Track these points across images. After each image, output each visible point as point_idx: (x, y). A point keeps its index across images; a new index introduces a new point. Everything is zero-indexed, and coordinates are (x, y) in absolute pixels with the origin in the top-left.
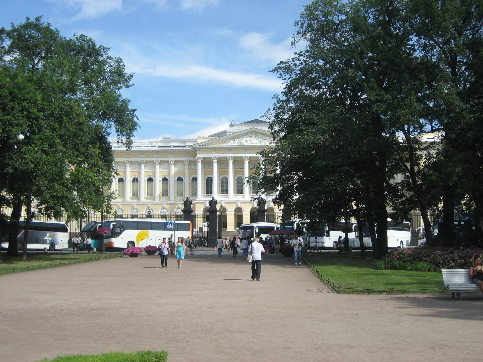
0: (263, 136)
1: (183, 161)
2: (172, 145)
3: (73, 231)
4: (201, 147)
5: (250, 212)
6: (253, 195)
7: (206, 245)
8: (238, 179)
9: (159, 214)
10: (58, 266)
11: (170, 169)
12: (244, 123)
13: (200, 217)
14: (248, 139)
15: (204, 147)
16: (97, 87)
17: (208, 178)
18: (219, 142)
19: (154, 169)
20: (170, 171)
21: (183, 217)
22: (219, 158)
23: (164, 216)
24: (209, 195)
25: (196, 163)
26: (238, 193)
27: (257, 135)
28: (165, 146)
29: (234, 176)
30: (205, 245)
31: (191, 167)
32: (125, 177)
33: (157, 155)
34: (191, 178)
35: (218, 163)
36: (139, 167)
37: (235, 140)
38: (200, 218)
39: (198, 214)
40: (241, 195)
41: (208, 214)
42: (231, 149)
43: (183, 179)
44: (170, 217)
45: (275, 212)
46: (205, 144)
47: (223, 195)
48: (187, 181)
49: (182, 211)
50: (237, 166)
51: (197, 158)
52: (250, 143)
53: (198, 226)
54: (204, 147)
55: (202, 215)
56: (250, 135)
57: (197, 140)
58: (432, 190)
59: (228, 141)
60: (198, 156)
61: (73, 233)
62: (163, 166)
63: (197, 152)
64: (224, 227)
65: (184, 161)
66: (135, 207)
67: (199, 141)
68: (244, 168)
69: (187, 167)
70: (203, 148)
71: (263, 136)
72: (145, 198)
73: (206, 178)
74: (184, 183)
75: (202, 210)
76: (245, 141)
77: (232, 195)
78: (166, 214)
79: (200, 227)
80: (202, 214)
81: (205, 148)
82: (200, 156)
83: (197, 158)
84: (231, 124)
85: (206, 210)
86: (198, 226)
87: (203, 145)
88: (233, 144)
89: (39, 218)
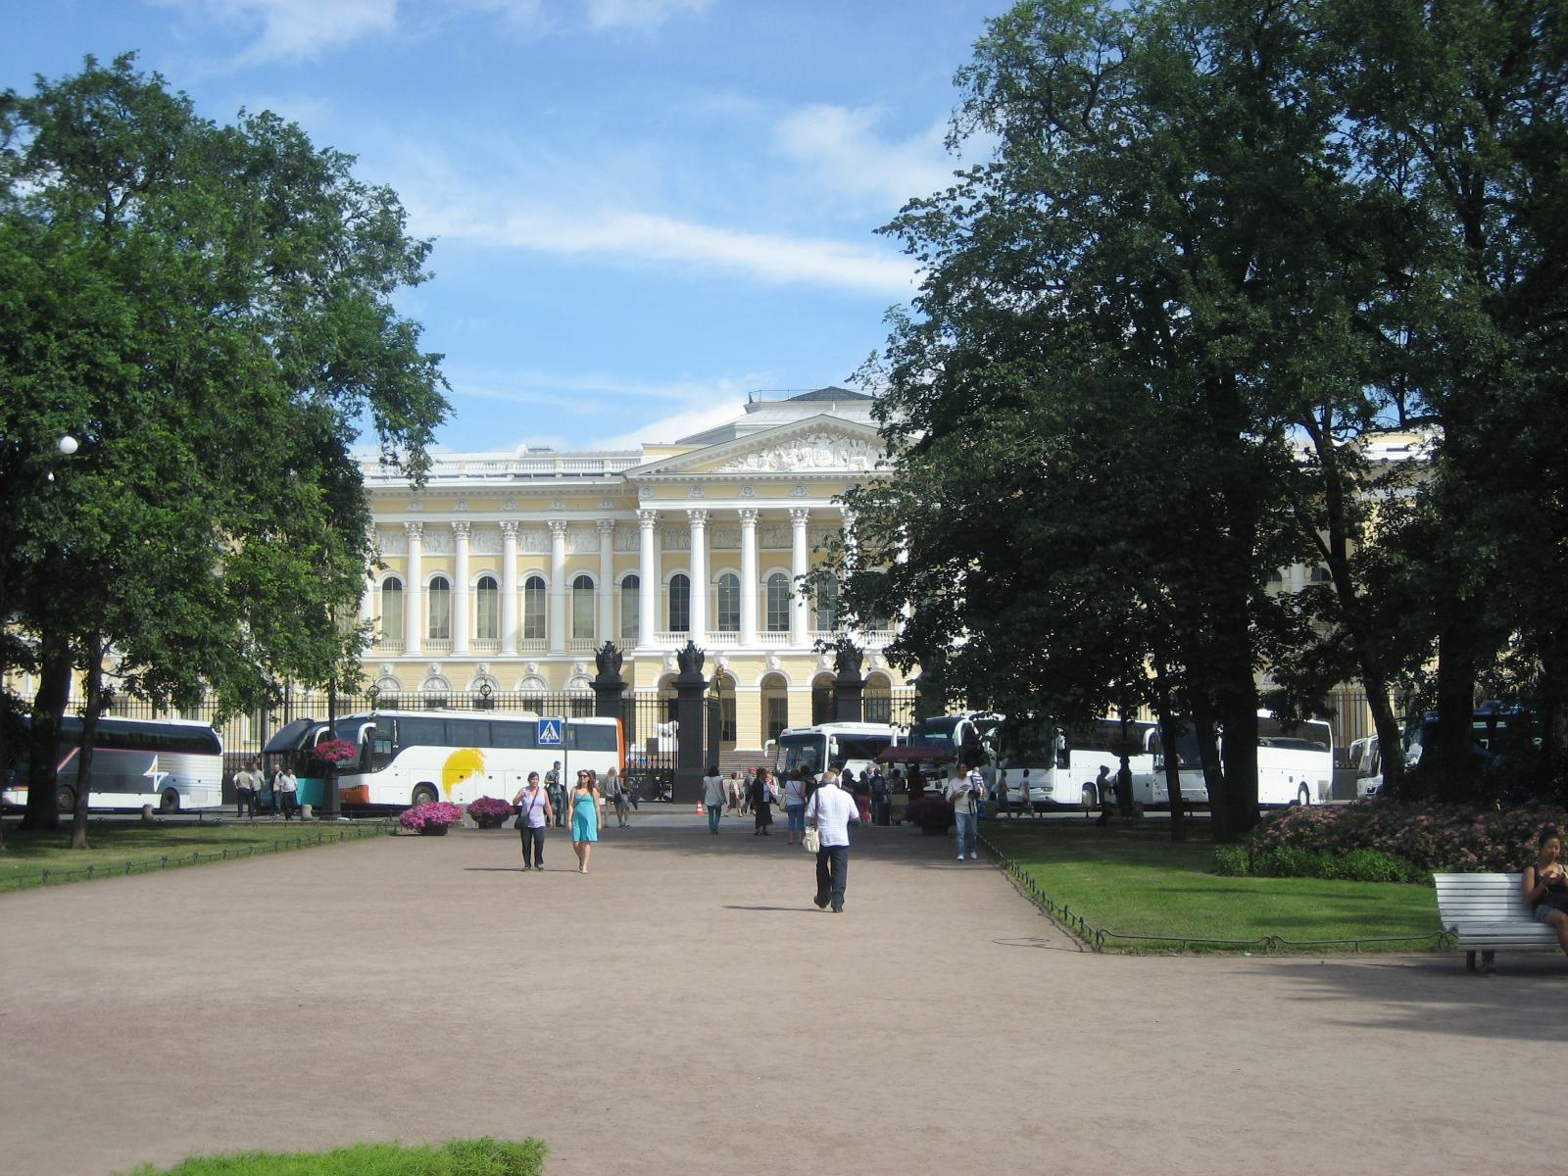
0: (854, 443)
1: (593, 525)
2: (557, 470)
3: (237, 751)
4: (653, 477)
5: (811, 689)
6: (822, 632)
8: (772, 581)
9: (518, 694)
10: (190, 864)
11: (551, 550)
12: (793, 399)
13: (649, 704)
14: (806, 450)
15: (662, 477)
18: (712, 461)
19: (499, 548)
20: (551, 556)
21: (594, 704)
22: (711, 514)
23: (531, 701)
24: (678, 633)
25: (635, 529)
26: (771, 628)
27: (834, 437)
28: (535, 475)
29: (760, 573)
30: (666, 797)
31: (621, 543)
32: (406, 574)
33: (509, 504)
34: (620, 580)
35: (709, 529)
36: (452, 544)
37: (764, 454)
38: (649, 710)
39: (644, 695)
40: (783, 632)
41: (674, 694)
42: (749, 485)
43: (595, 582)
44: (551, 704)
45: (892, 688)
46: (666, 469)
47: (723, 632)
48: (606, 587)
50: (769, 539)
51: (638, 512)
52: (811, 463)
53: (644, 735)
54: (662, 477)
55: (655, 698)
56: (812, 438)
57: (641, 454)
58: (1401, 616)
59: (740, 459)
60: (644, 505)
61: (237, 757)
62: (530, 540)
63: (640, 494)
64: (726, 738)
65: (598, 523)
66: (535, 672)
67: (647, 459)
68: (791, 547)
69: (606, 541)
70: (658, 480)
71: (854, 443)
72: (472, 642)
73: (668, 579)
74: (599, 595)
76: (795, 460)
78: (540, 694)
79: (649, 736)
80: (655, 695)
81: (665, 480)
82: (648, 505)
83: (638, 512)
84: (751, 401)
85: (668, 682)
86: (644, 735)
87: (658, 472)
88: (755, 469)
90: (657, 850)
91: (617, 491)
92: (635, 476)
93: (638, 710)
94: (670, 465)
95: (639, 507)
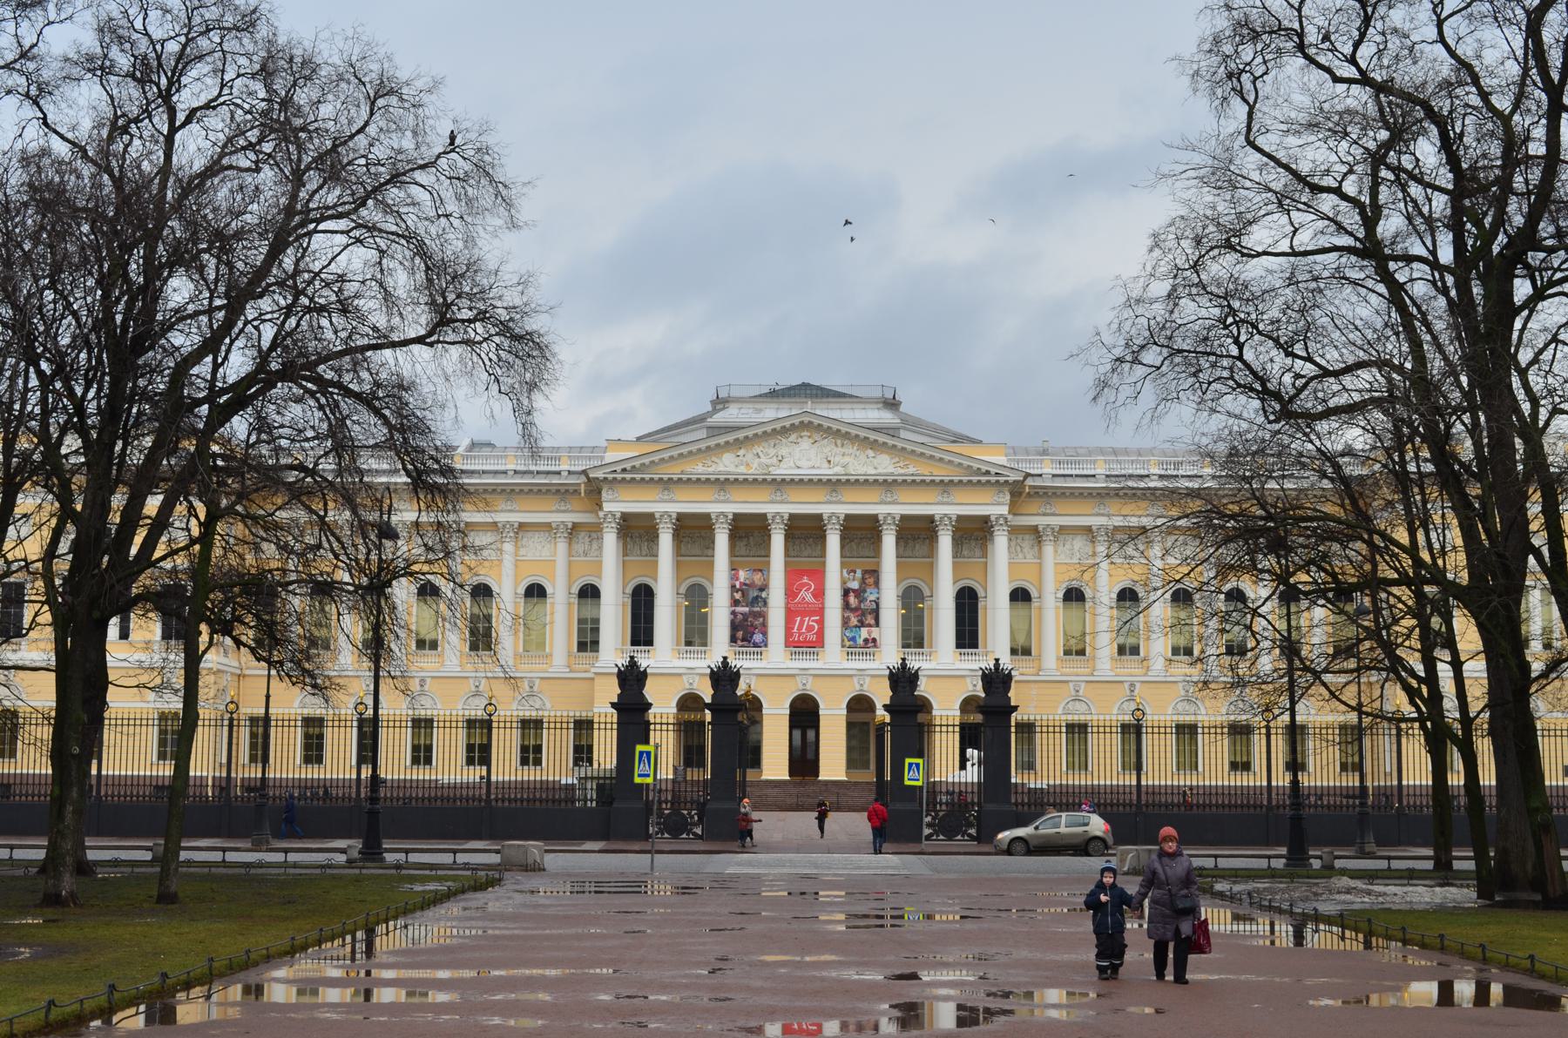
1: (547, 527)
2: (1045, 471)
3: (1115, 783)
4: (619, 476)
5: (788, 712)
6: (636, 648)
7: (973, 831)
9: (461, 713)
12: (760, 396)
16: (246, 264)
17: (693, 586)
21: (1013, 729)
22: (737, 517)
23: (475, 721)
24: (966, 650)
25: (595, 530)
26: (688, 643)
27: (817, 436)
28: (538, 472)
30: (695, 834)
31: (579, 547)
35: (790, 537)
36: (1036, 549)
39: (944, 719)
40: (647, 648)
41: (977, 718)
42: (723, 484)
43: (549, 590)
44: (280, 723)
45: (934, 712)
47: (689, 648)
49: (613, 705)
50: (741, 544)
52: (792, 464)
54: (629, 476)
55: (671, 721)
56: (793, 437)
57: (605, 450)
60: (607, 507)
61: (551, 786)
63: (604, 494)
64: (752, 767)
65: (554, 525)
67: (610, 457)
68: (768, 556)
69: (562, 546)
73: (629, 590)
74: (553, 604)
75: (674, 704)
77: (833, 655)
78: (1032, 718)
80: (671, 716)
81: (630, 477)
83: (601, 514)
85: (968, 704)
87: (624, 470)
88: (732, 469)
89: (160, 719)
92: (599, 474)
94: (637, 463)
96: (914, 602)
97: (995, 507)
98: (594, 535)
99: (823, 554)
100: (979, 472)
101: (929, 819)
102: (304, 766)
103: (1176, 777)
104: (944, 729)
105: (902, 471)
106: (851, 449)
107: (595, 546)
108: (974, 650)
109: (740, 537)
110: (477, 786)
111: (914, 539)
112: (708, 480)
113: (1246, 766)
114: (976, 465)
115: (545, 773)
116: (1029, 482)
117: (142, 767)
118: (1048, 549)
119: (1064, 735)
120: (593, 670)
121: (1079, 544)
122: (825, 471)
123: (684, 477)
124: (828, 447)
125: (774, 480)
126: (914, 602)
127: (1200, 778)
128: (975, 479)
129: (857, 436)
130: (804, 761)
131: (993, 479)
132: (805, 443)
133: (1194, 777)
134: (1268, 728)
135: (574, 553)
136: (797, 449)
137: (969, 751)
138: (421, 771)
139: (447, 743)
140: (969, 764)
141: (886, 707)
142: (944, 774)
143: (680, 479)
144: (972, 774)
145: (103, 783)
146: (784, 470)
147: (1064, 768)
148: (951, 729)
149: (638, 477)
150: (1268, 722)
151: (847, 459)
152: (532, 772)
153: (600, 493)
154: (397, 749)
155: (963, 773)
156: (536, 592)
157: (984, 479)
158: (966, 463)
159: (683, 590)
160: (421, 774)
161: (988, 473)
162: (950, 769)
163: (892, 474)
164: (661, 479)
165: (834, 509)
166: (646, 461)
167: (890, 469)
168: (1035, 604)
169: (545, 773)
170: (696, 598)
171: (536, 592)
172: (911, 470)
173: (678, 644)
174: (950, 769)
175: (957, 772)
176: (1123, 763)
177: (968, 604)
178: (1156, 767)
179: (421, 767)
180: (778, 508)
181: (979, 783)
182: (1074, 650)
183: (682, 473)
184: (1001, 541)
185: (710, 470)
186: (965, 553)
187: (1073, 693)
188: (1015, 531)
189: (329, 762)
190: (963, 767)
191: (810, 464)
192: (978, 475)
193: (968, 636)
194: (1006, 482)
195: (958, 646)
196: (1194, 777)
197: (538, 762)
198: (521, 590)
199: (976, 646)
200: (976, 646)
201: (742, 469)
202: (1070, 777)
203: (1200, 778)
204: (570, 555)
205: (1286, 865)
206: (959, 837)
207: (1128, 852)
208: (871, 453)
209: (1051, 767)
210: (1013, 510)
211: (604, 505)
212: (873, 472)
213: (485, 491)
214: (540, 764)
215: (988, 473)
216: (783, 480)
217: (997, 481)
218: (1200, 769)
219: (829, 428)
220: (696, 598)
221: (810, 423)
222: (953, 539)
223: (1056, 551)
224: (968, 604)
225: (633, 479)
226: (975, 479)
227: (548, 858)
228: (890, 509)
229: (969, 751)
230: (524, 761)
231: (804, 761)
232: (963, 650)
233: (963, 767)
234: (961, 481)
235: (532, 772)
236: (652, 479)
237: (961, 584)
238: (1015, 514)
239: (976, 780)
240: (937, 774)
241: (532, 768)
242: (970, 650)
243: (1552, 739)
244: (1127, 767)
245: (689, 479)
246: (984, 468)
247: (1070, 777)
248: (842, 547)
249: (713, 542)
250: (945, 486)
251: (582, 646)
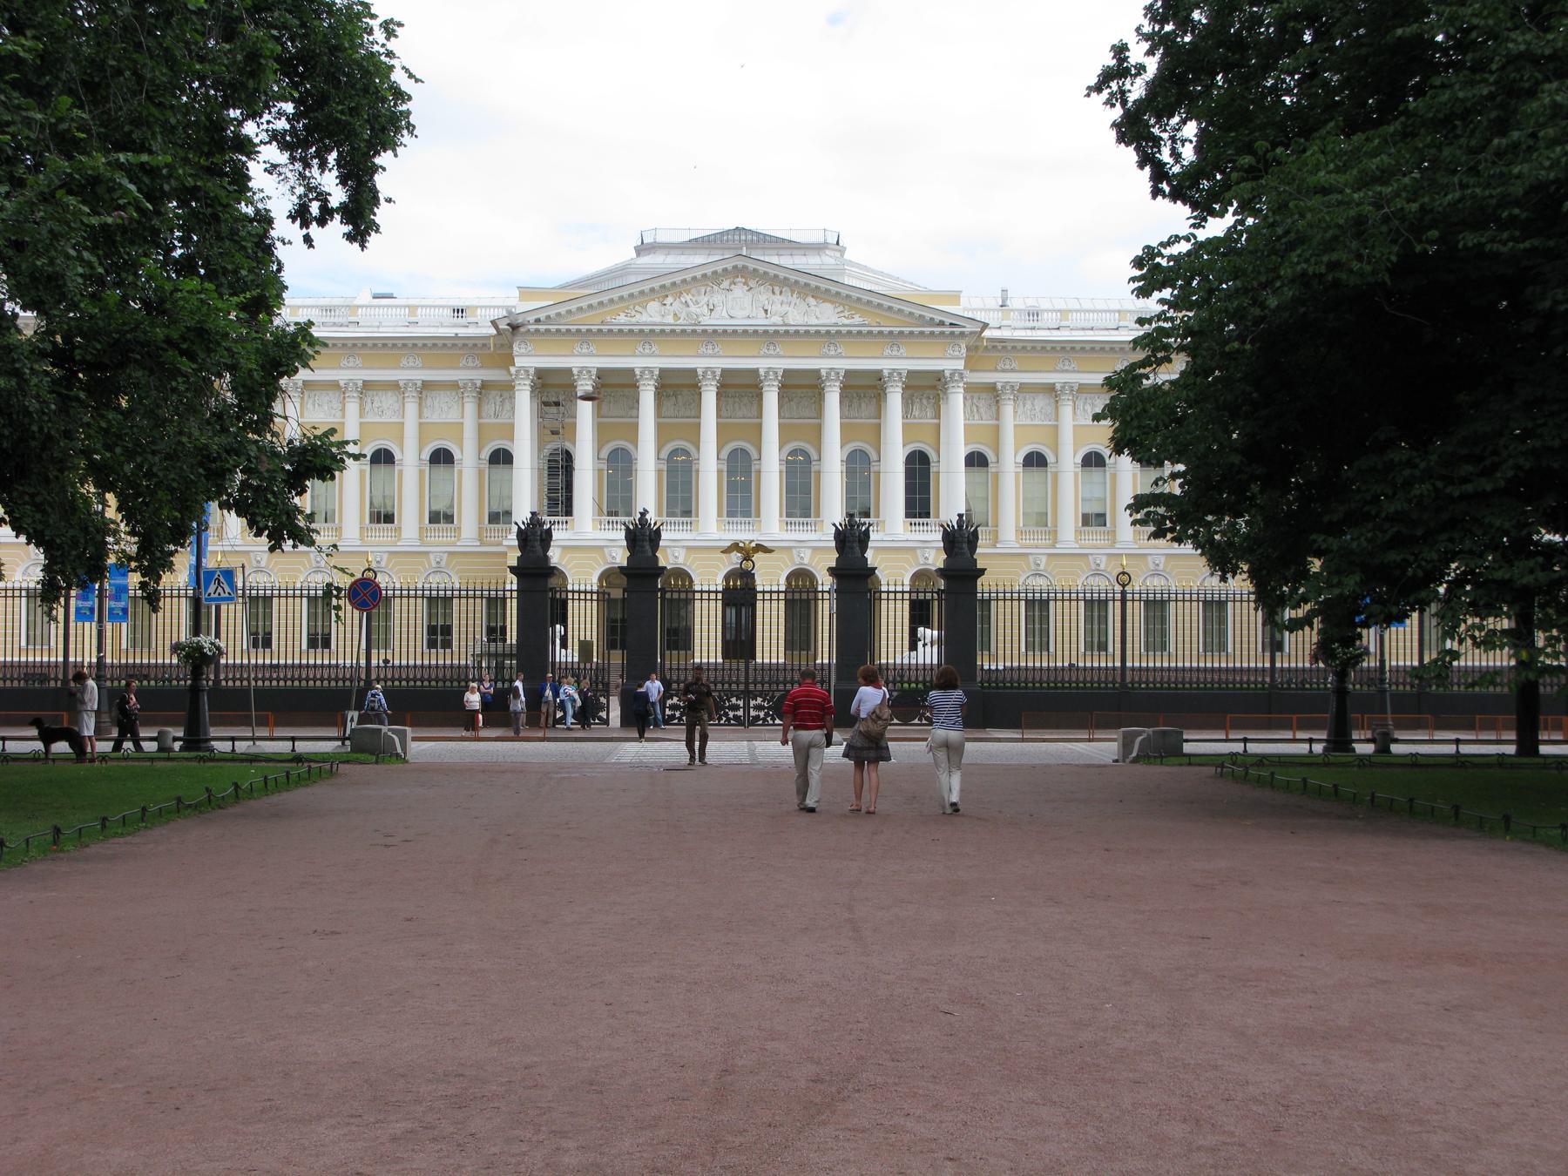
0: (777, 290)
1: (454, 386)
8: (733, 454)
10: (196, 807)
11: (997, 419)
13: (899, 596)
14: (717, 298)
15: (542, 327)
18: (613, 307)
19: (339, 414)
20: (1056, 427)
24: (917, 520)
25: (507, 389)
27: (752, 283)
29: (600, 441)
32: (997, 446)
33: (351, 359)
34: (486, 454)
36: (994, 408)
37: (669, 300)
38: (775, 604)
46: (548, 317)
48: (469, 458)
51: (513, 370)
52: (724, 314)
53: (1408, 629)
54: (542, 327)
56: (726, 284)
58: (307, 483)
59: (637, 308)
60: (519, 362)
62: (1028, 406)
63: (516, 348)
66: (263, 564)
68: (699, 417)
69: (470, 407)
70: (537, 331)
71: (777, 290)
72: (1019, 532)
76: (706, 310)
77: (771, 525)
79: (582, 638)
82: (528, 359)
84: (642, 243)
86: (1408, 629)
88: (657, 319)
90: (1212, 752)
91: (484, 345)
93: (759, 605)
94: (552, 313)
95: (514, 365)
96: (860, 469)
97: (950, 363)
98: (506, 394)
99: (819, 413)
100: (931, 322)
101: (1434, 687)
102: (252, 650)
103: (1202, 659)
104: (705, 596)
105: (846, 322)
106: (787, 295)
107: (507, 406)
108: (925, 520)
109: (668, 396)
110: (720, 667)
111: (860, 398)
112: (631, 331)
113: (1103, 647)
114: (928, 315)
115: (456, 656)
116: (987, 333)
117: (1300, 659)
118: (1008, 409)
119: (595, 603)
120: (505, 543)
121: (1041, 403)
122: (760, 321)
123: (605, 328)
124: (764, 296)
125: (705, 331)
126: (860, 469)
127: (1110, 659)
128: (927, 330)
129: (797, 282)
130: (739, 642)
131: (948, 330)
132: (739, 291)
133: (1045, 658)
134: (1123, 593)
135: (484, 414)
136: (730, 296)
137: (921, 630)
138: (319, 656)
139: (405, 622)
140: (920, 644)
141: (832, 571)
142: (705, 654)
143: (600, 331)
144: (928, 655)
145: (557, 666)
146: (719, 320)
147: (1023, 649)
148: (713, 596)
149: (553, 328)
150: (1124, 586)
151: (785, 308)
152: (441, 656)
153: (511, 347)
154: (1245, 646)
155: (913, 654)
156: (442, 458)
157: (937, 330)
158: (917, 312)
159: (605, 454)
160: (319, 658)
161: (942, 323)
162: (899, 649)
163: (836, 325)
164: (579, 331)
165: (770, 363)
166: (563, 310)
167: (834, 320)
168: (992, 468)
169: (456, 656)
170: (619, 466)
171: (442, 458)
172: (857, 319)
173: (600, 512)
174: (899, 649)
175: (906, 653)
176: (1147, 643)
177: (919, 469)
178: (412, 636)
179: (319, 650)
180: (708, 362)
181: (939, 664)
182: (1041, 520)
183: (602, 323)
184: (957, 401)
185: (633, 320)
186: (916, 413)
187: (1093, 566)
188: (971, 389)
189: (397, 643)
190: (913, 646)
191: (746, 313)
192: (931, 326)
193: (919, 504)
194: (962, 334)
195: (908, 515)
196: (1045, 658)
197: (447, 644)
198: (426, 455)
199: (928, 515)
200: (928, 515)
201: (670, 319)
202: (1030, 659)
203: (1110, 659)
204: (480, 417)
205: (1325, 749)
206: (916, 721)
207: (1140, 733)
208: (812, 301)
209: (412, 636)
210: (971, 364)
211: (516, 359)
212: (816, 322)
213: (364, 345)
214: (1106, 650)
215: (942, 323)
216: (715, 331)
217: (952, 333)
218: (1052, 649)
219: (765, 273)
220: (619, 466)
221: (745, 267)
222: (903, 398)
223: (1015, 412)
224: (919, 469)
225: (548, 331)
226: (927, 330)
227: (414, 747)
228: (833, 363)
229: (921, 630)
230: (432, 644)
231: (739, 642)
232: (913, 520)
233: (913, 646)
234: (911, 333)
235: (441, 656)
236: (558, 331)
237: (910, 448)
238: (971, 371)
239: (935, 661)
240: (884, 655)
241: (441, 651)
242: (921, 520)
243: (1008, 603)
244: (1209, 648)
245: (610, 331)
246: (938, 318)
247: (1030, 659)
248: (718, 399)
249: (638, 402)
250: (895, 338)
251: (435, 518)
